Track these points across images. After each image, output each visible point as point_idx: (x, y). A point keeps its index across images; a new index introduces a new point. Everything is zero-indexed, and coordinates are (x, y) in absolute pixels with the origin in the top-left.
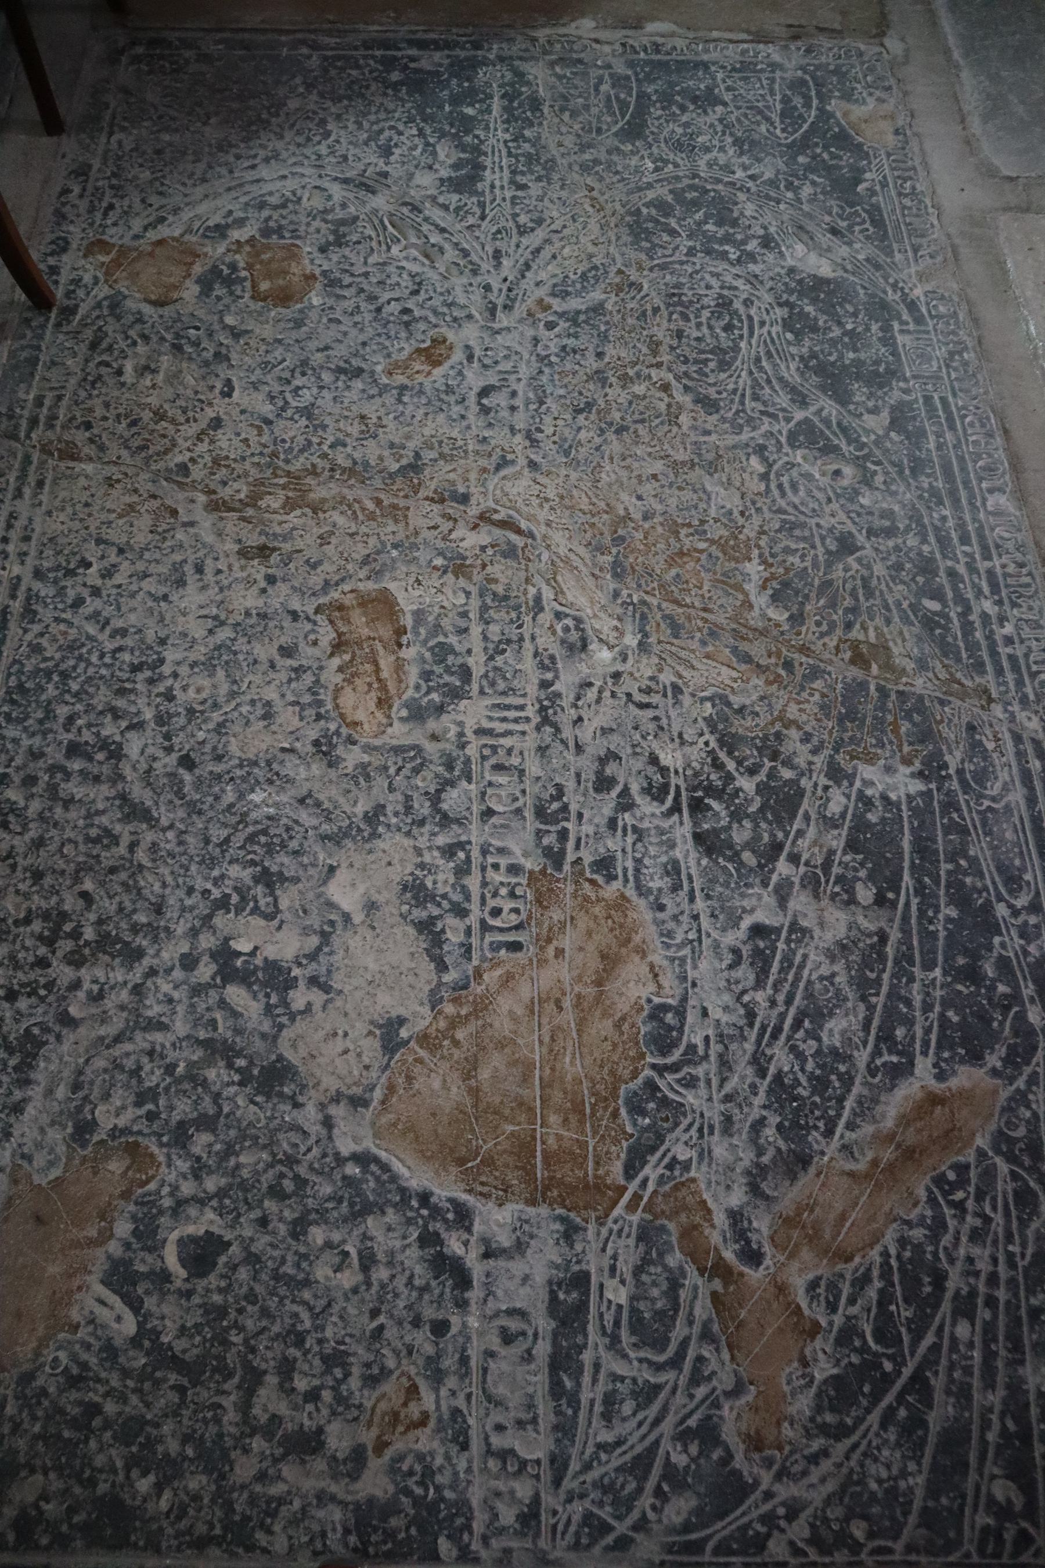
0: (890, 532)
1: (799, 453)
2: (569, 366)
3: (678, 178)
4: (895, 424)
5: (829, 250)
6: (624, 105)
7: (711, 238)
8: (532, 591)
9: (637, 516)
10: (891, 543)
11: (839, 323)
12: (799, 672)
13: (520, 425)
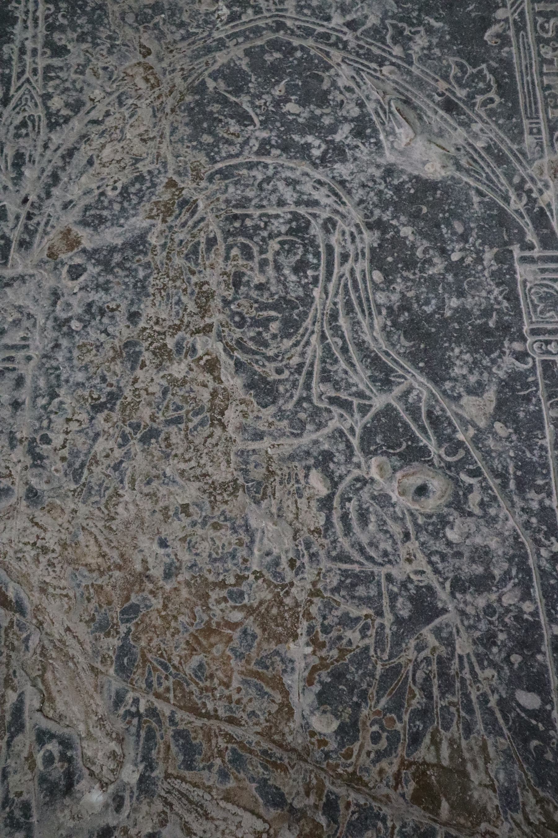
0: (482, 583)
1: (374, 461)
2: (94, 335)
3: (257, 31)
4: (504, 410)
5: (441, 134)
7: (290, 126)
8: (12, 697)
9: (157, 572)
10: (481, 602)
11: (444, 252)
12: (345, 816)
13: (23, 433)
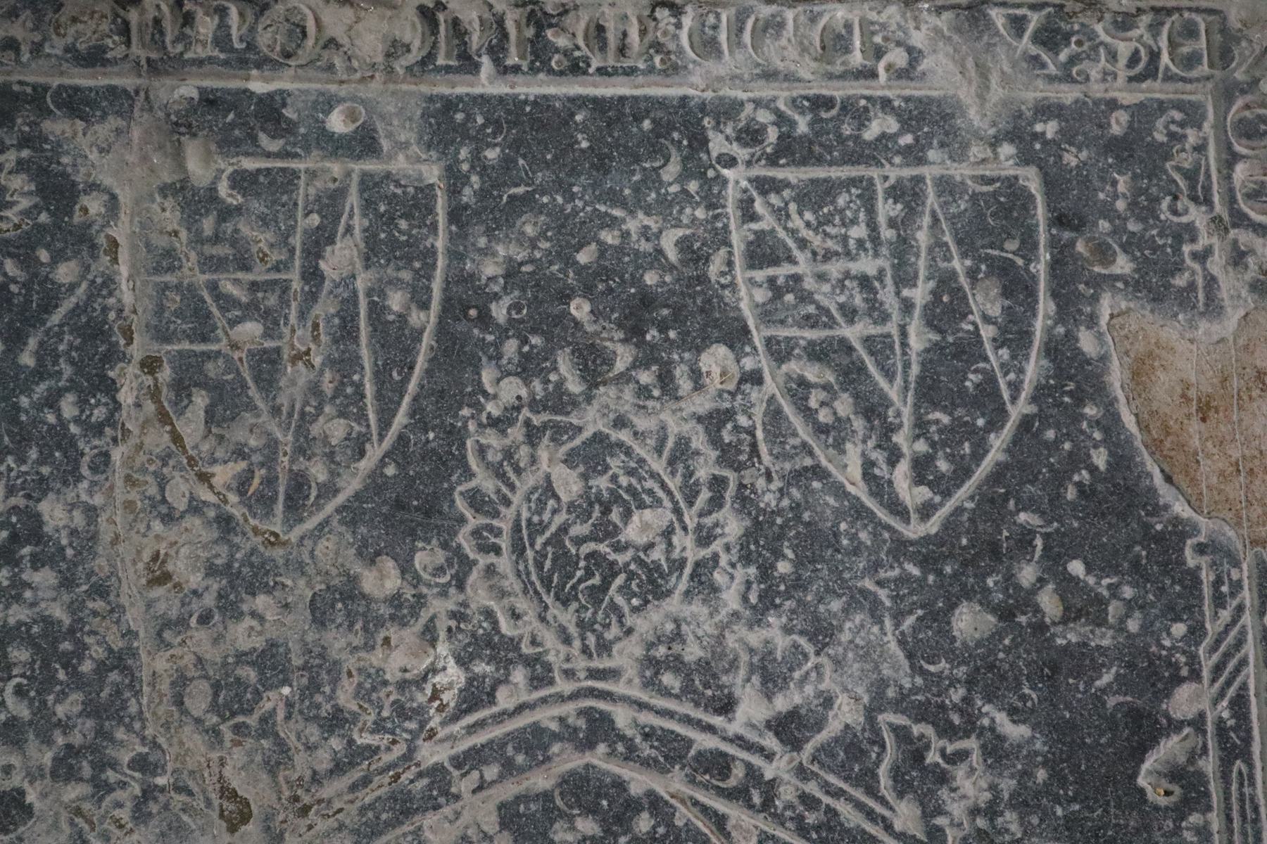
6: (395, 340)
